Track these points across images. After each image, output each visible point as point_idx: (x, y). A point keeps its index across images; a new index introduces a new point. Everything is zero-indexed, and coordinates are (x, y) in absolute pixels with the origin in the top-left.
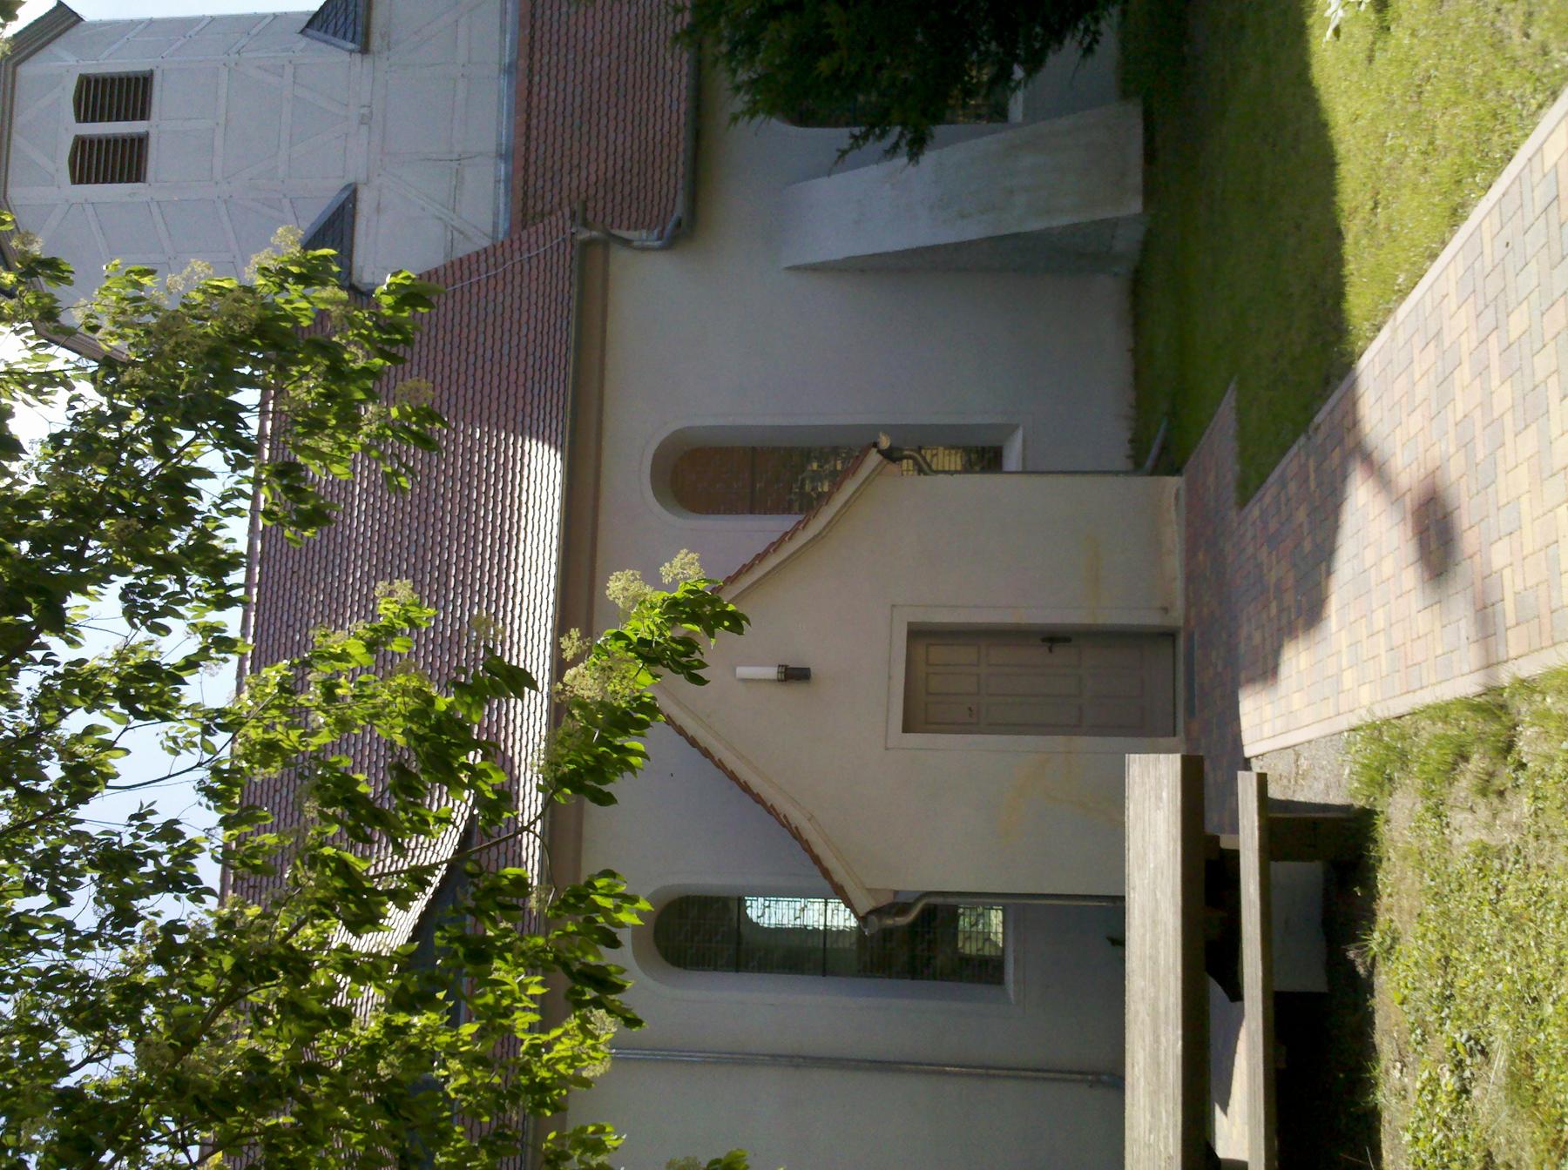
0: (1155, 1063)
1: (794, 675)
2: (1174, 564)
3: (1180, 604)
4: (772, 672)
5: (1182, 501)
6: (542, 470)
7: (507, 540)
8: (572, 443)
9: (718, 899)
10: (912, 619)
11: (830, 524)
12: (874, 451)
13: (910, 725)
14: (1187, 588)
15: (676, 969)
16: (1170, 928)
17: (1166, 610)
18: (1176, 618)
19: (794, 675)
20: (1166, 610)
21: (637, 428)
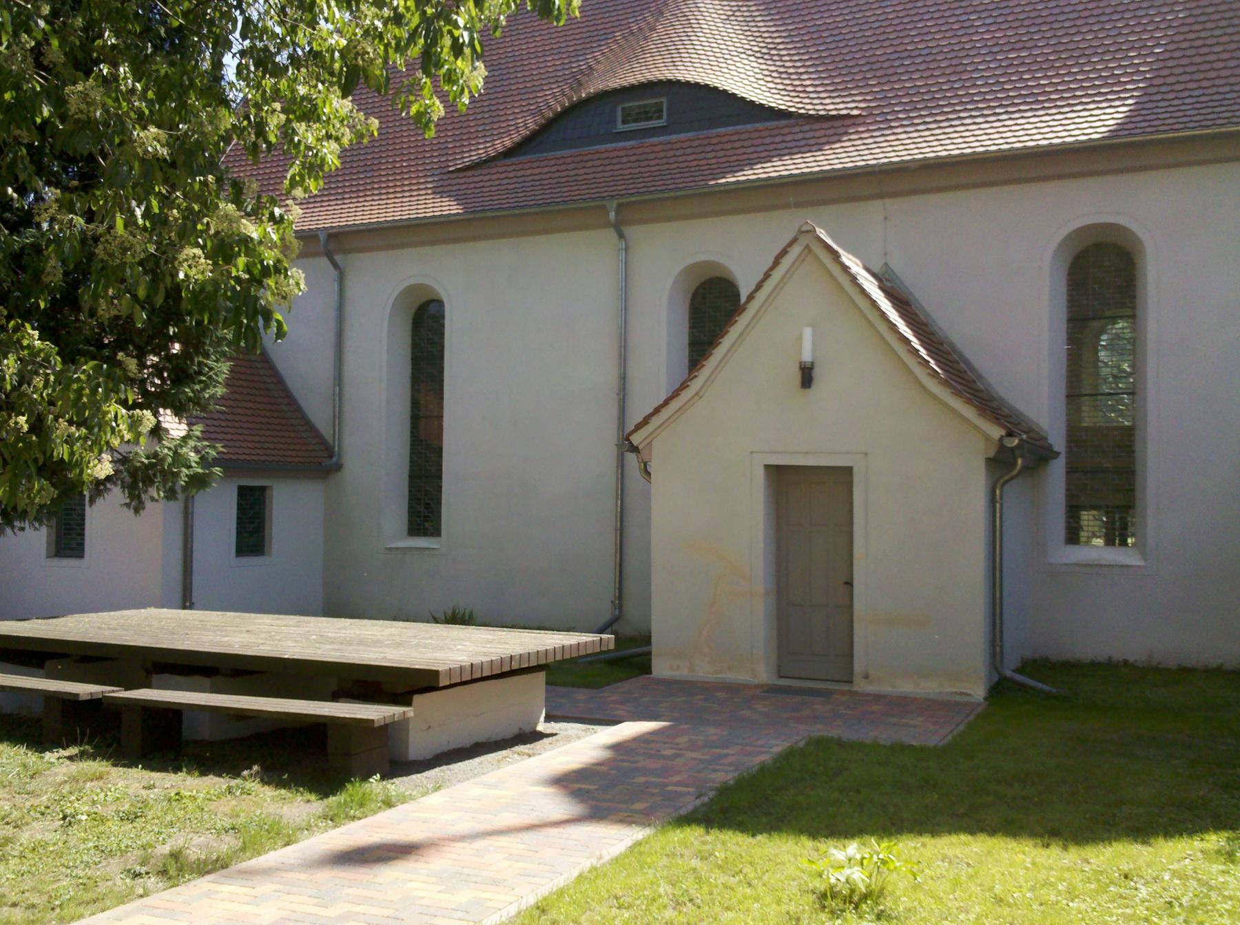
0: (361, 642)
1: (807, 376)
2: (905, 687)
3: (872, 688)
4: (807, 357)
5: (958, 698)
6: (1094, 121)
7: (1037, 100)
8: (1111, 147)
9: (1133, 297)
10: (855, 471)
11: (935, 397)
12: (1003, 432)
13: (848, 471)
14: (868, 695)
15: (410, 322)
16: (439, 655)
17: (866, 677)
18: (860, 686)
19: (807, 376)
20: (866, 677)
21: (1140, 206)
